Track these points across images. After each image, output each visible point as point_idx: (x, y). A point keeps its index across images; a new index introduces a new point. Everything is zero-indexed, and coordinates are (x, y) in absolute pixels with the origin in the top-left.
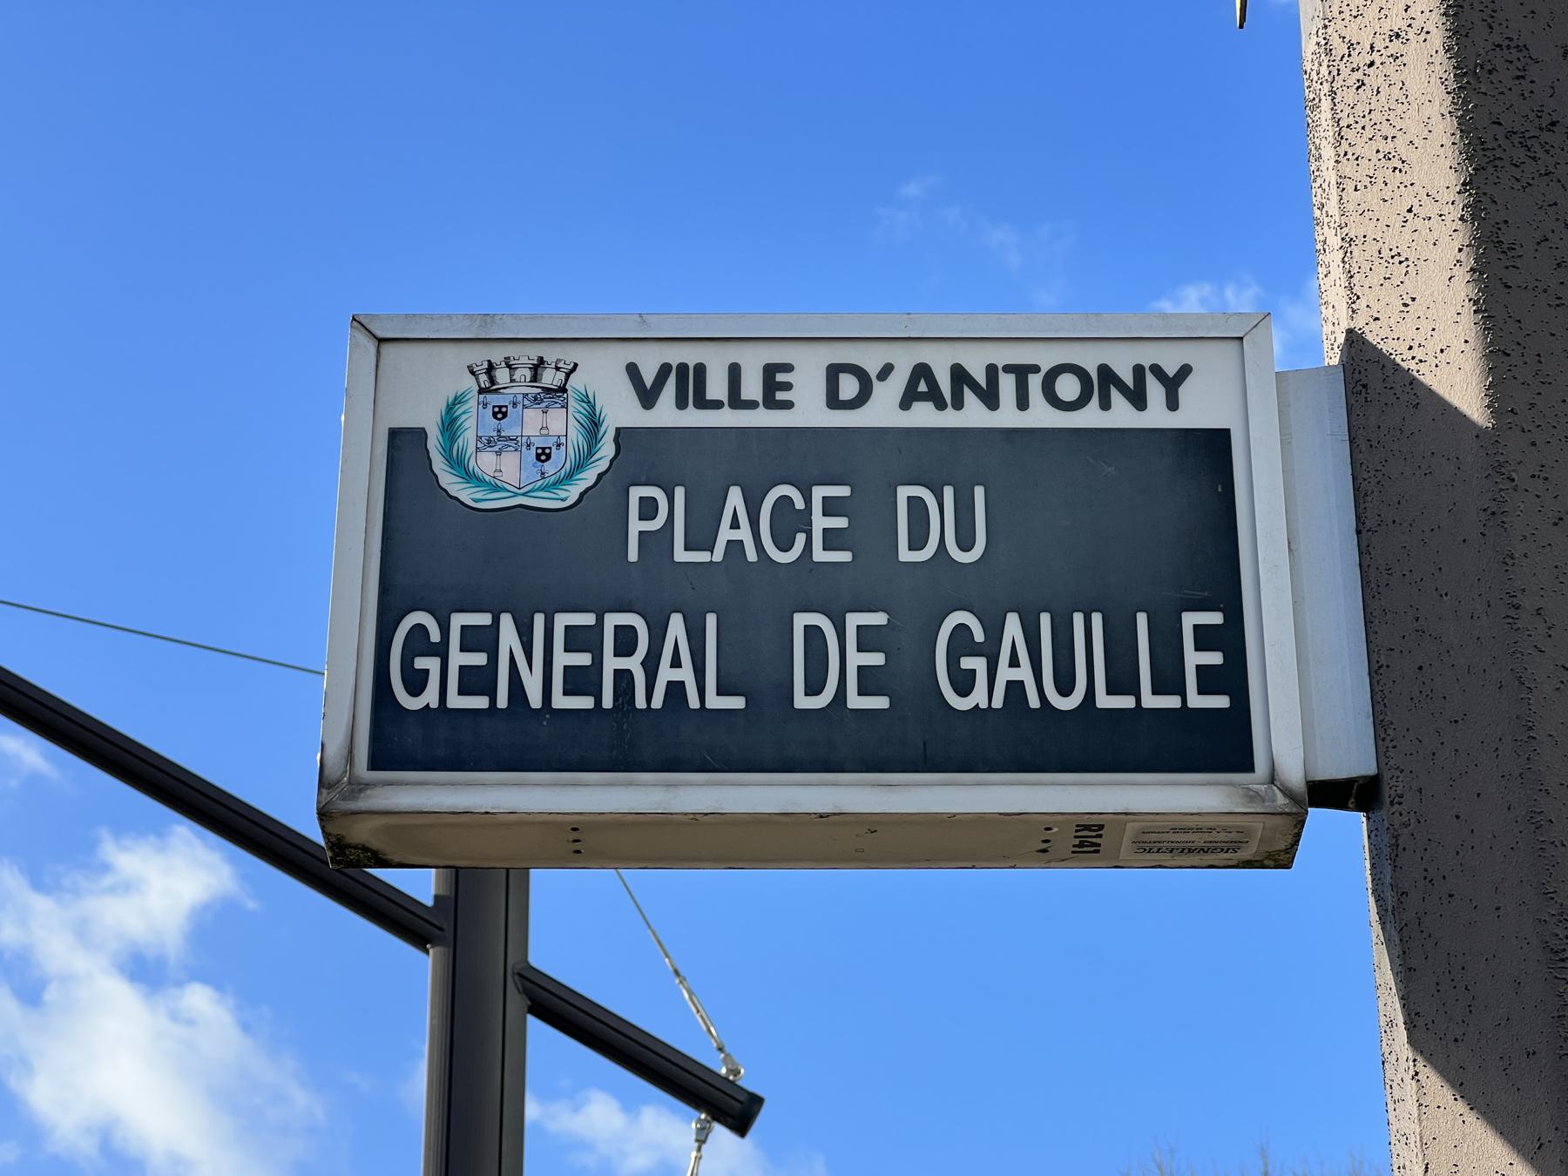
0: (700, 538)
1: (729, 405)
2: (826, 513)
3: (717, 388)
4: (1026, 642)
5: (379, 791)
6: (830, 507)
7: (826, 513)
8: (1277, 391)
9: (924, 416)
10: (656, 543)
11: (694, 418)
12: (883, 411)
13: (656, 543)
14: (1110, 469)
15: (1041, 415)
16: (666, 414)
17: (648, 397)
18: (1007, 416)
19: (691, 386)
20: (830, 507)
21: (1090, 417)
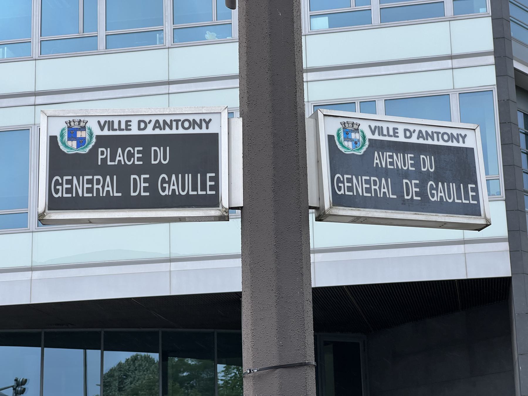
0: (113, 159)
3: (116, 126)
10: (104, 160)
11: (112, 133)
13: (104, 160)
16: (376, 137)
17: (102, 129)
18: (174, 131)
19: (381, 133)
21: (191, 131)
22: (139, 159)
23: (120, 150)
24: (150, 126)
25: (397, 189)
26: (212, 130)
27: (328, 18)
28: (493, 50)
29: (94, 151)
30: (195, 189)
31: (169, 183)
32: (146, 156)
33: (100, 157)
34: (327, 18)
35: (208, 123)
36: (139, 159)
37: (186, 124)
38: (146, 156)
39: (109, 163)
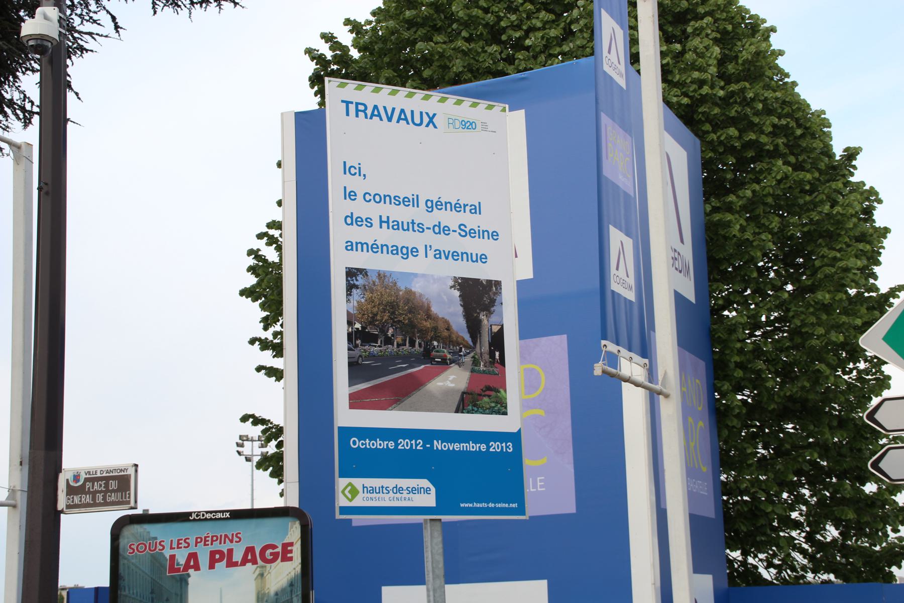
0: (93, 488)
1: (271, 473)
2: (540, 482)
3: (91, 473)
4: (10, 461)
5: (630, 138)
6: (541, 481)
7: (540, 482)
8: (280, 293)
9: (108, 475)
10: (89, 488)
11: (90, 476)
12: (104, 475)
13: (89, 488)
14: (750, 155)
15: (116, 474)
16: (88, 476)
17: (86, 474)
18: (114, 474)
19: (90, 474)
20: (541, 481)
21: (120, 474)
22: (541, 487)
23: (96, 483)
24: (105, 473)
25: (94, 499)
26: (128, 473)
27: (568, 337)
28: (620, 370)
29: (84, 484)
30: (122, 498)
31: (111, 496)
32: (107, 486)
33: (87, 487)
34: (566, 338)
35: (127, 470)
36: (541, 487)
37: (119, 471)
38: (107, 486)
39: (91, 490)
